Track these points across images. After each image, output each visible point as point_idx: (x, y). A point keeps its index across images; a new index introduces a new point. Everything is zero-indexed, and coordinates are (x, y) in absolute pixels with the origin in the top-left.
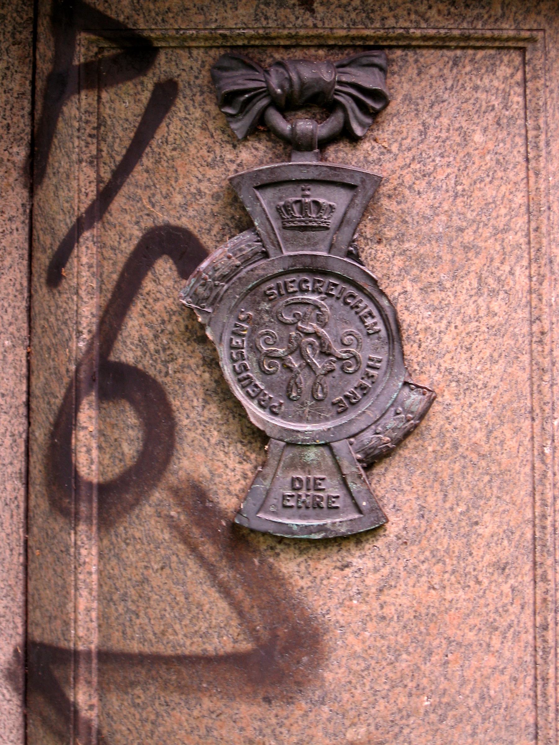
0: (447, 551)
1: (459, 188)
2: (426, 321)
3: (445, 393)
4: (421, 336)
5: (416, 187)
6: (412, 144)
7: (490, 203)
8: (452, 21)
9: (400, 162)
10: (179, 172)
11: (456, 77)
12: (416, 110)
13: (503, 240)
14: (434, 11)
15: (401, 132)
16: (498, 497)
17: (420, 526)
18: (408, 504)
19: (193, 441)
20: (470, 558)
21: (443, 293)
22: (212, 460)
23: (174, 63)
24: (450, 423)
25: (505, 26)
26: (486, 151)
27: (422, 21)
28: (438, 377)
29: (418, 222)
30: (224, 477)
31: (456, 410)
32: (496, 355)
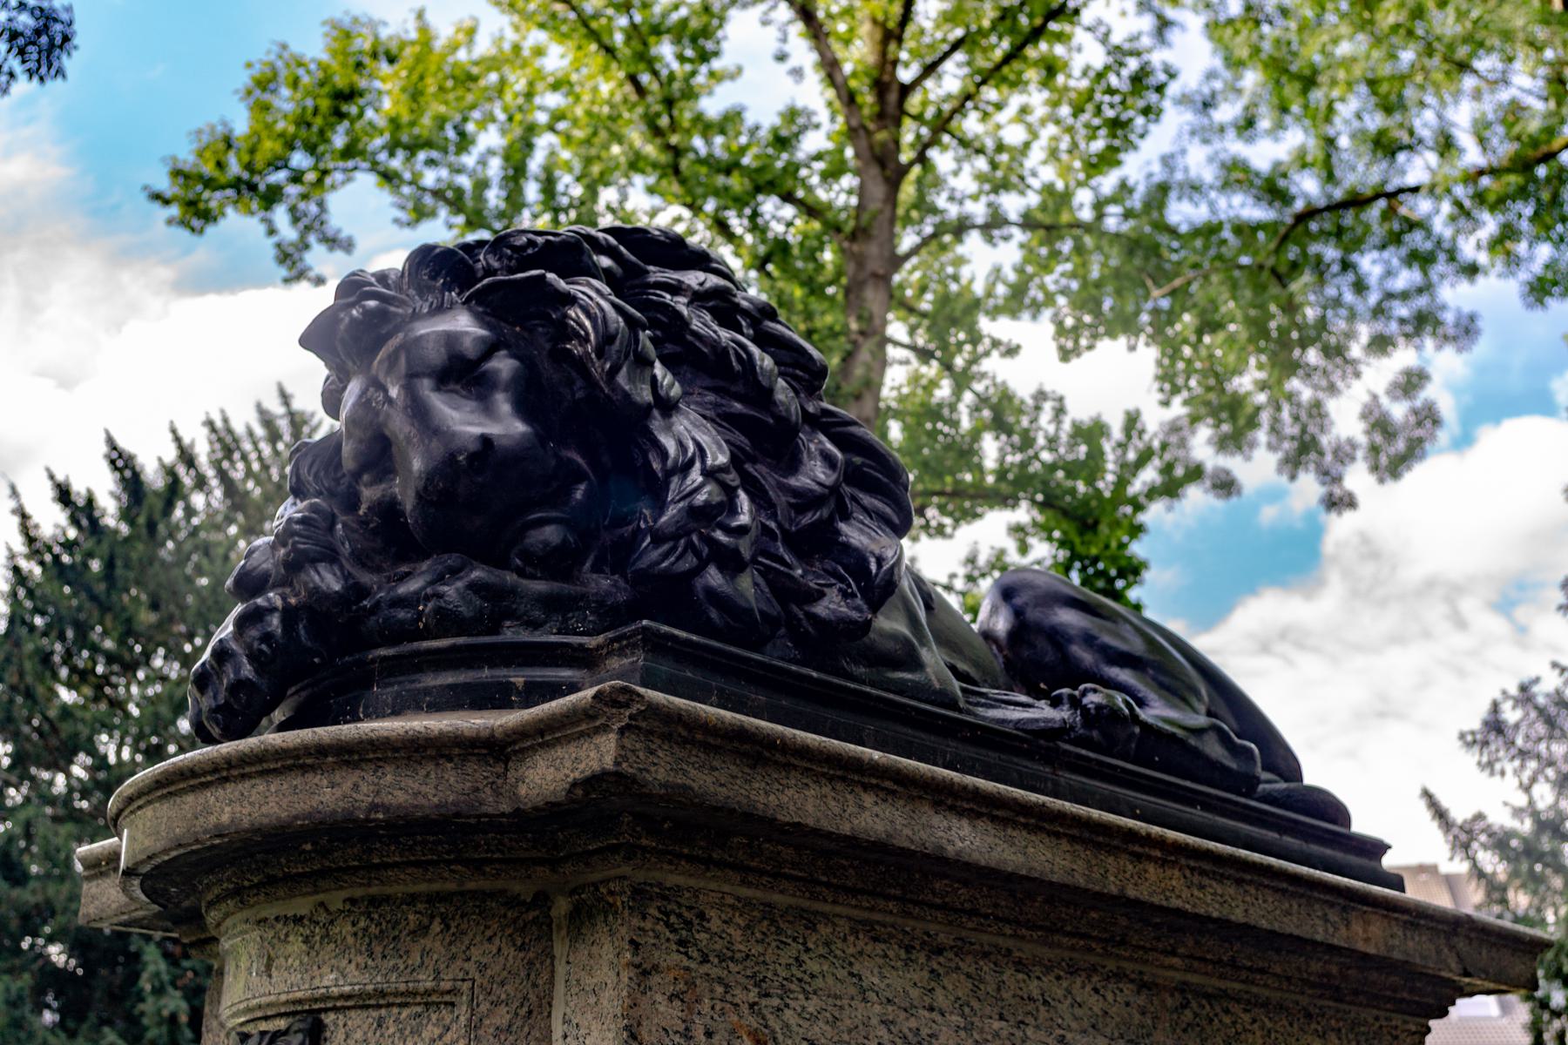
14: (353, 966)
25: (421, 977)
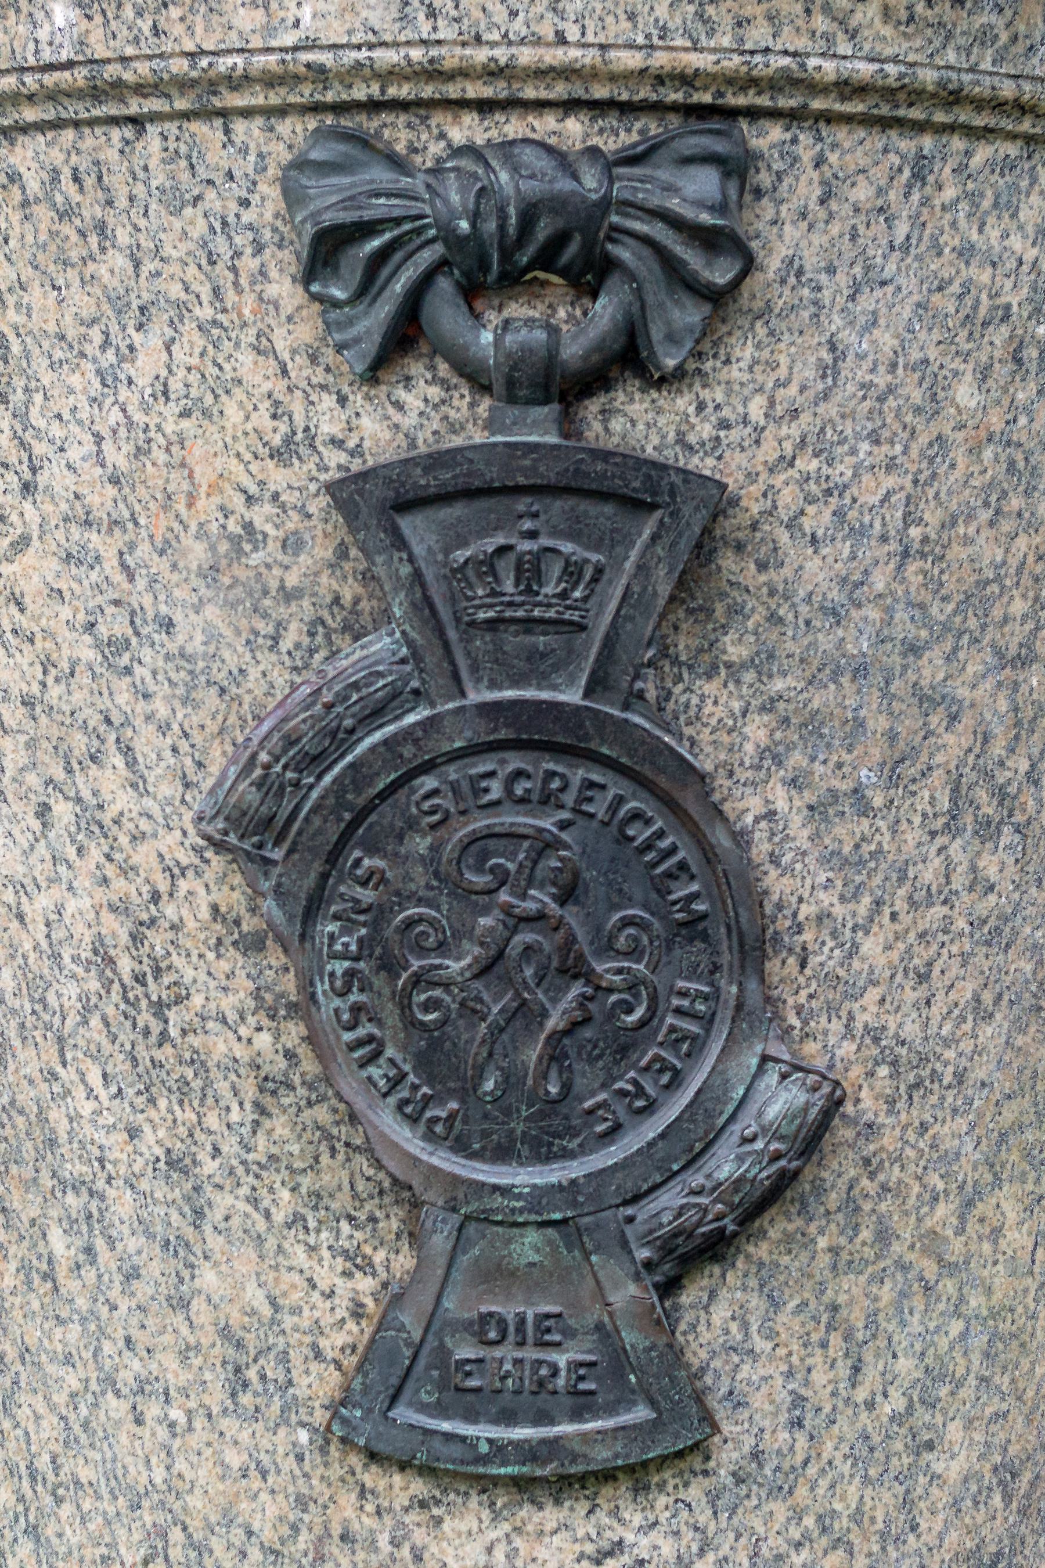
0: (857, 1516)
1: (915, 532)
2: (822, 895)
3: (863, 1094)
4: (807, 936)
5: (807, 523)
6: (800, 400)
7: (988, 582)
8: (918, 43)
9: (768, 452)
10: (197, 475)
11: (918, 215)
12: (815, 303)
13: (1016, 684)
15: (775, 366)
16: (983, 1379)
17: (792, 1449)
18: (764, 1389)
19: (227, 1219)
20: (911, 1538)
21: (865, 823)
22: (276, 1268)
23: (183, 163)
24: (872, 1176)
26: (983, 434)
27: (840, 36)
28: (848, 1049)
29: (808, 623)
30: (306, 1312)
31: (889, 1140)
32: (987, 997)
